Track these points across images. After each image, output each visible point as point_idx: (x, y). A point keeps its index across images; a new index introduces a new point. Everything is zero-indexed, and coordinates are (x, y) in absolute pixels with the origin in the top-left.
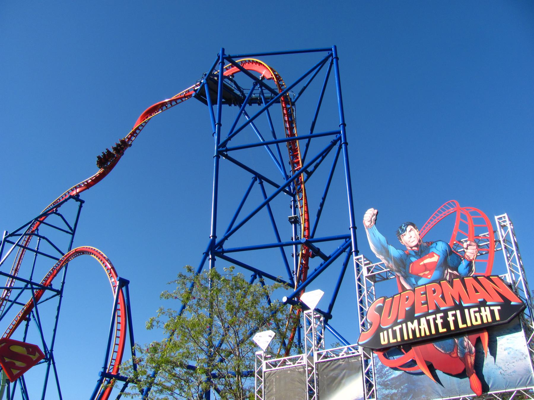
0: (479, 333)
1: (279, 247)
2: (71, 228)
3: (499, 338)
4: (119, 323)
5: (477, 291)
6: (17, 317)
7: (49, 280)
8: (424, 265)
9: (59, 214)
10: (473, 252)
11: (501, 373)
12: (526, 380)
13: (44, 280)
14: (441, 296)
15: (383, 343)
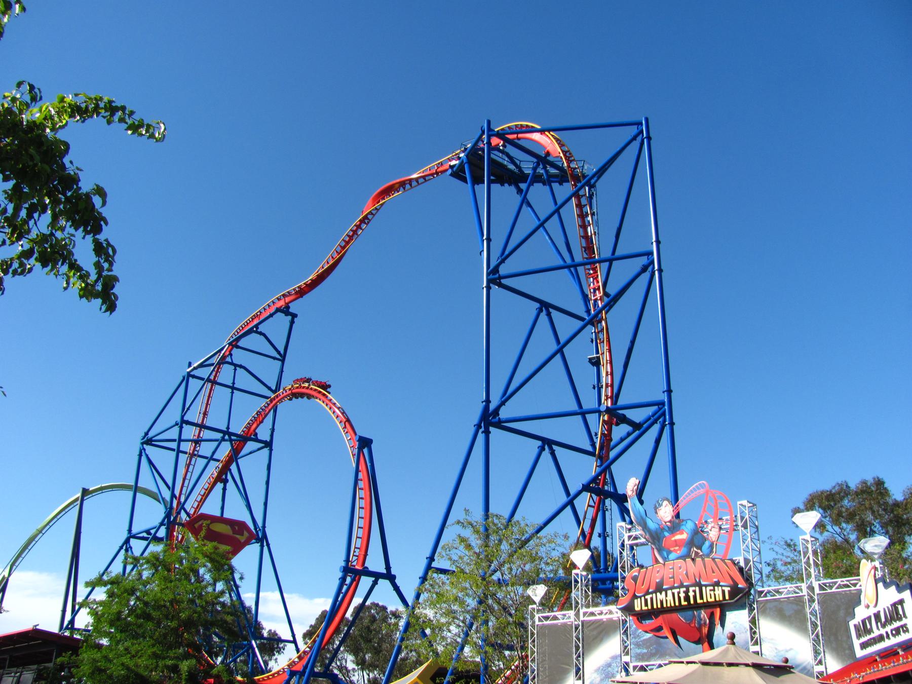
2: (279, 353)
4: (362, 498)
5: (713, 572)
6: (210, 478)
7: (254, 426)
8: (675, 541)
9: (261, 333)
13: (245, 427)
14: (685, 572)
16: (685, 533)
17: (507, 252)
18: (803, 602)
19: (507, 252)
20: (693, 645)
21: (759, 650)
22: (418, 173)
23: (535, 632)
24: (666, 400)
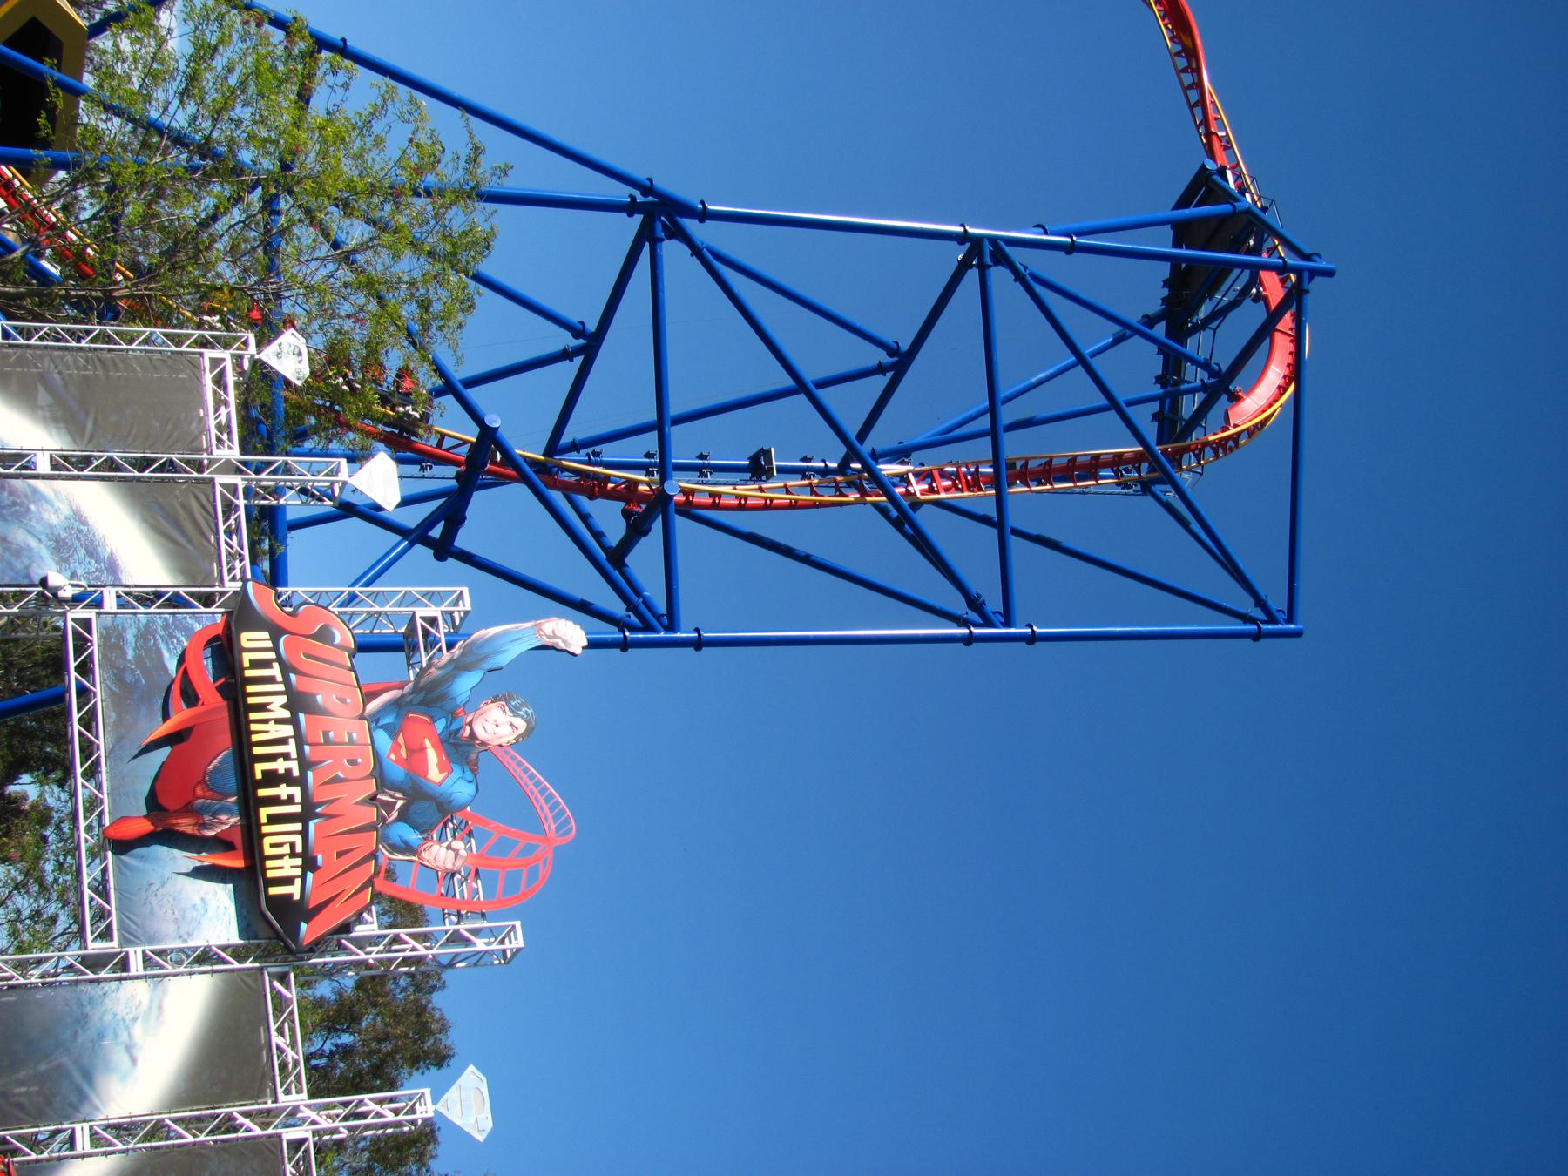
0: (244, 849)
1: (655, 418)
3: (230, 891)
5: (340, 854)
8: (423, 749)
10: (439, 861)
11: (152, 884)
12: (132, 931)
14: (341, 775)
15: (245, 636)
16: (443, 775)
17: (1038, 289)
18: (258, 1097)
19: (1038, 289)
20: (145, 788)
21: (133, 972)
22: (1212, 91)
23: (183, 349)
24: (679, 635)
